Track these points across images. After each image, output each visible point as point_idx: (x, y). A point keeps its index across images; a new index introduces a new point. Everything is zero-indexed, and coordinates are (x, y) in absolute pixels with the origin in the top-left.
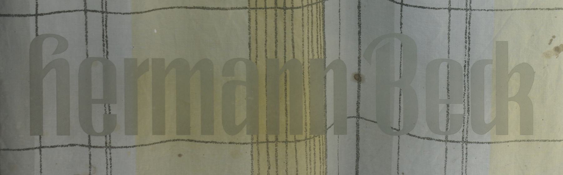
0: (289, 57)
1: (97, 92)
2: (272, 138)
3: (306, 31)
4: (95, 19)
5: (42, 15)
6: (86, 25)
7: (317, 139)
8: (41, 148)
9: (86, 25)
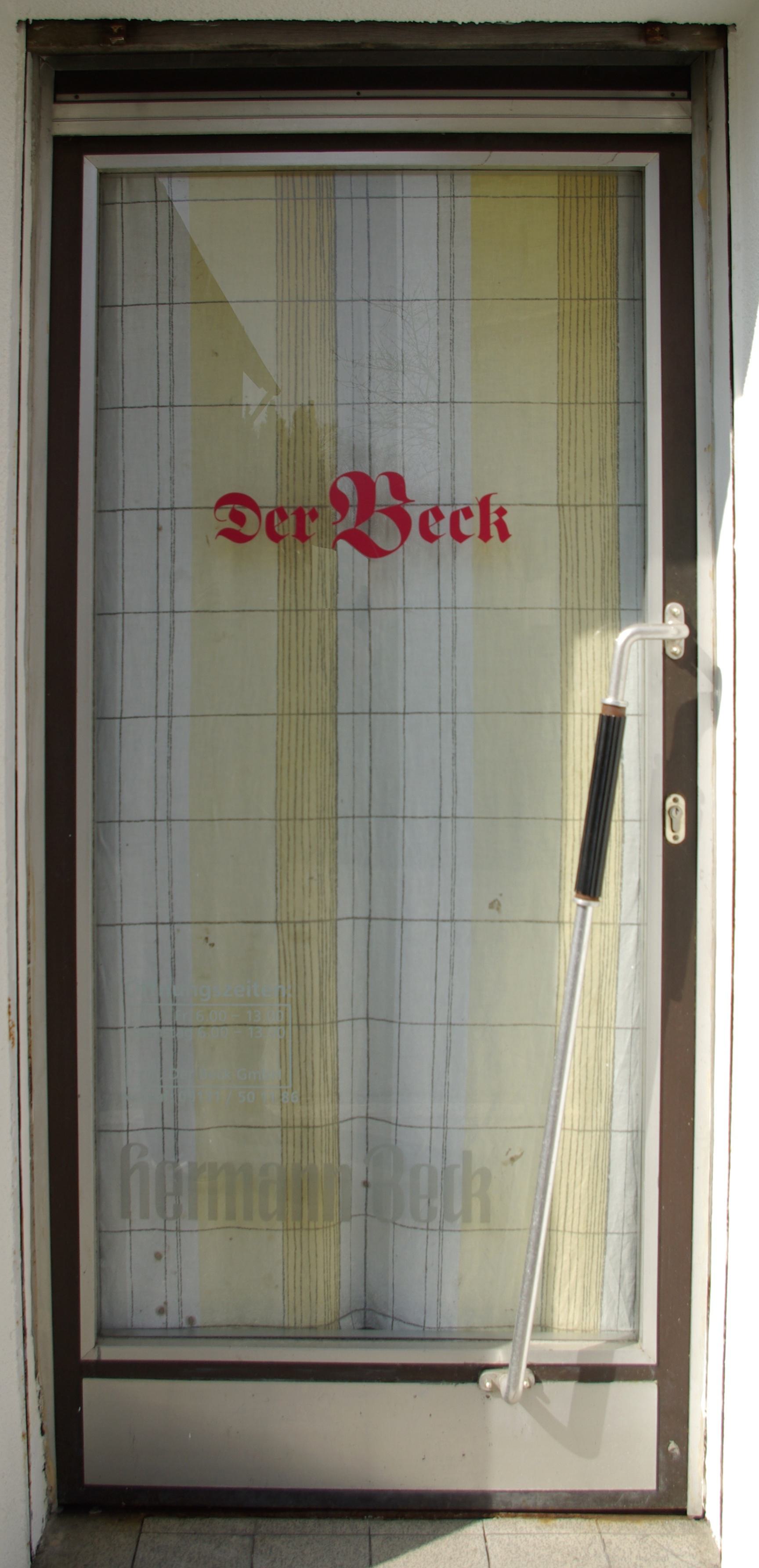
0: (311, 1161)
1: (170, 1187)
2: (298, 1226)
3: (324, 1145)
4: (170, 1134)
5: (132, 1130)
6: (163, 1138)
7: (344, 1226)
8: (130, 1231)
9: (163, 1138)
